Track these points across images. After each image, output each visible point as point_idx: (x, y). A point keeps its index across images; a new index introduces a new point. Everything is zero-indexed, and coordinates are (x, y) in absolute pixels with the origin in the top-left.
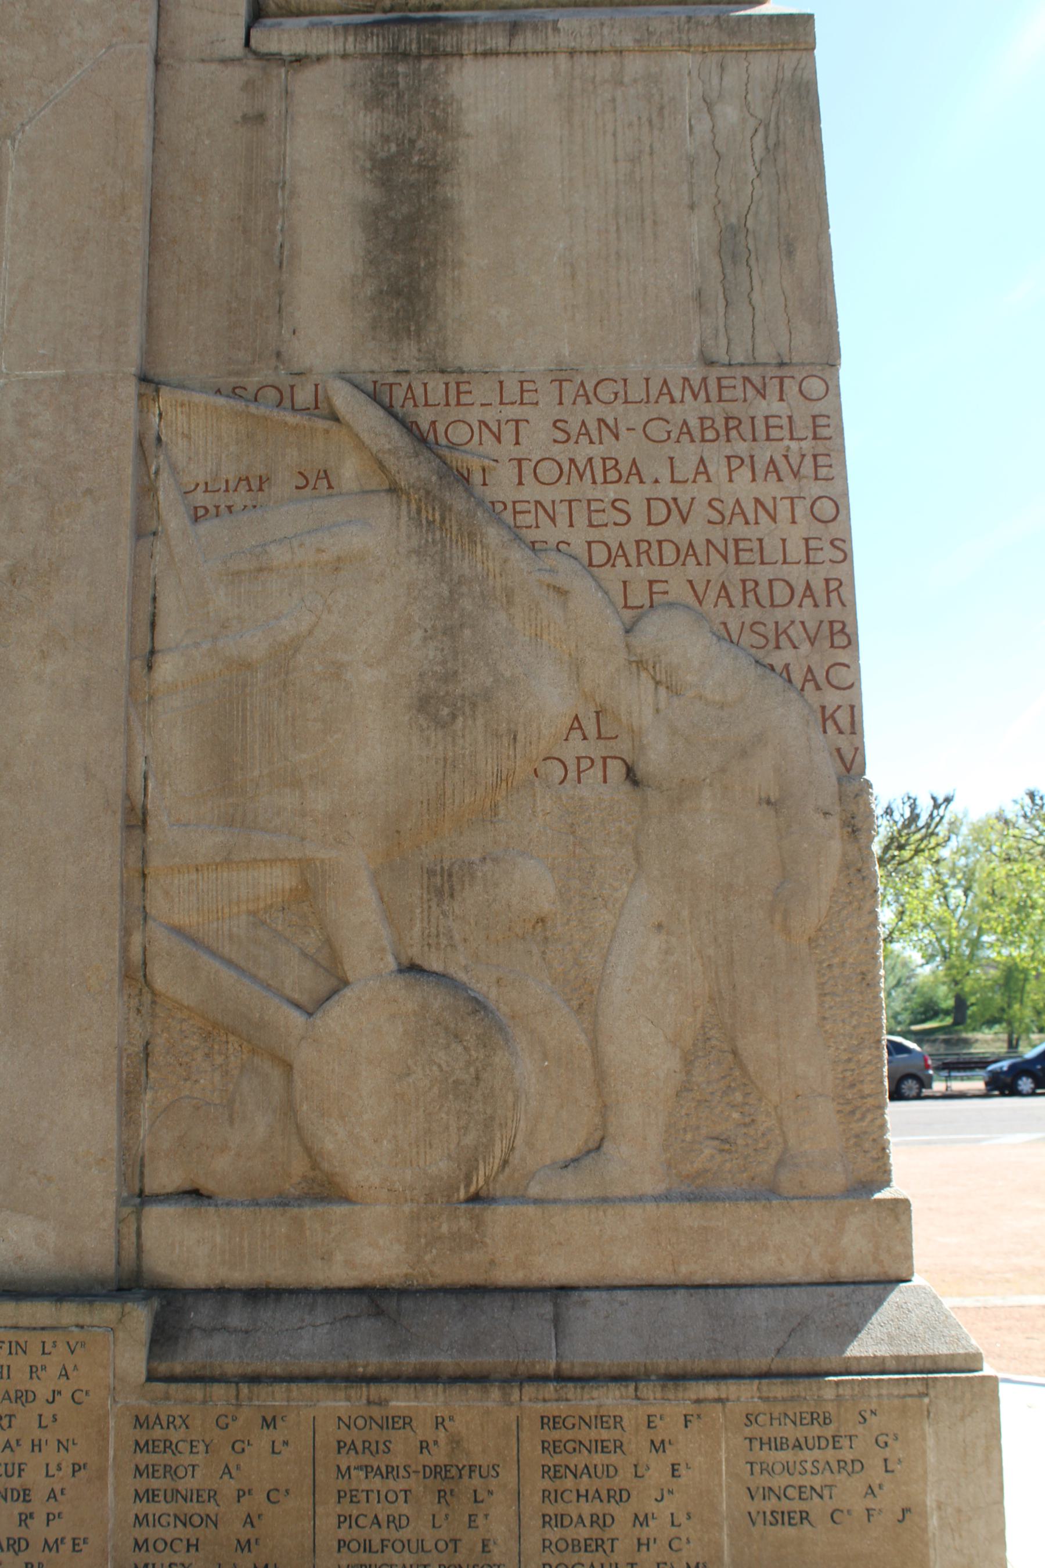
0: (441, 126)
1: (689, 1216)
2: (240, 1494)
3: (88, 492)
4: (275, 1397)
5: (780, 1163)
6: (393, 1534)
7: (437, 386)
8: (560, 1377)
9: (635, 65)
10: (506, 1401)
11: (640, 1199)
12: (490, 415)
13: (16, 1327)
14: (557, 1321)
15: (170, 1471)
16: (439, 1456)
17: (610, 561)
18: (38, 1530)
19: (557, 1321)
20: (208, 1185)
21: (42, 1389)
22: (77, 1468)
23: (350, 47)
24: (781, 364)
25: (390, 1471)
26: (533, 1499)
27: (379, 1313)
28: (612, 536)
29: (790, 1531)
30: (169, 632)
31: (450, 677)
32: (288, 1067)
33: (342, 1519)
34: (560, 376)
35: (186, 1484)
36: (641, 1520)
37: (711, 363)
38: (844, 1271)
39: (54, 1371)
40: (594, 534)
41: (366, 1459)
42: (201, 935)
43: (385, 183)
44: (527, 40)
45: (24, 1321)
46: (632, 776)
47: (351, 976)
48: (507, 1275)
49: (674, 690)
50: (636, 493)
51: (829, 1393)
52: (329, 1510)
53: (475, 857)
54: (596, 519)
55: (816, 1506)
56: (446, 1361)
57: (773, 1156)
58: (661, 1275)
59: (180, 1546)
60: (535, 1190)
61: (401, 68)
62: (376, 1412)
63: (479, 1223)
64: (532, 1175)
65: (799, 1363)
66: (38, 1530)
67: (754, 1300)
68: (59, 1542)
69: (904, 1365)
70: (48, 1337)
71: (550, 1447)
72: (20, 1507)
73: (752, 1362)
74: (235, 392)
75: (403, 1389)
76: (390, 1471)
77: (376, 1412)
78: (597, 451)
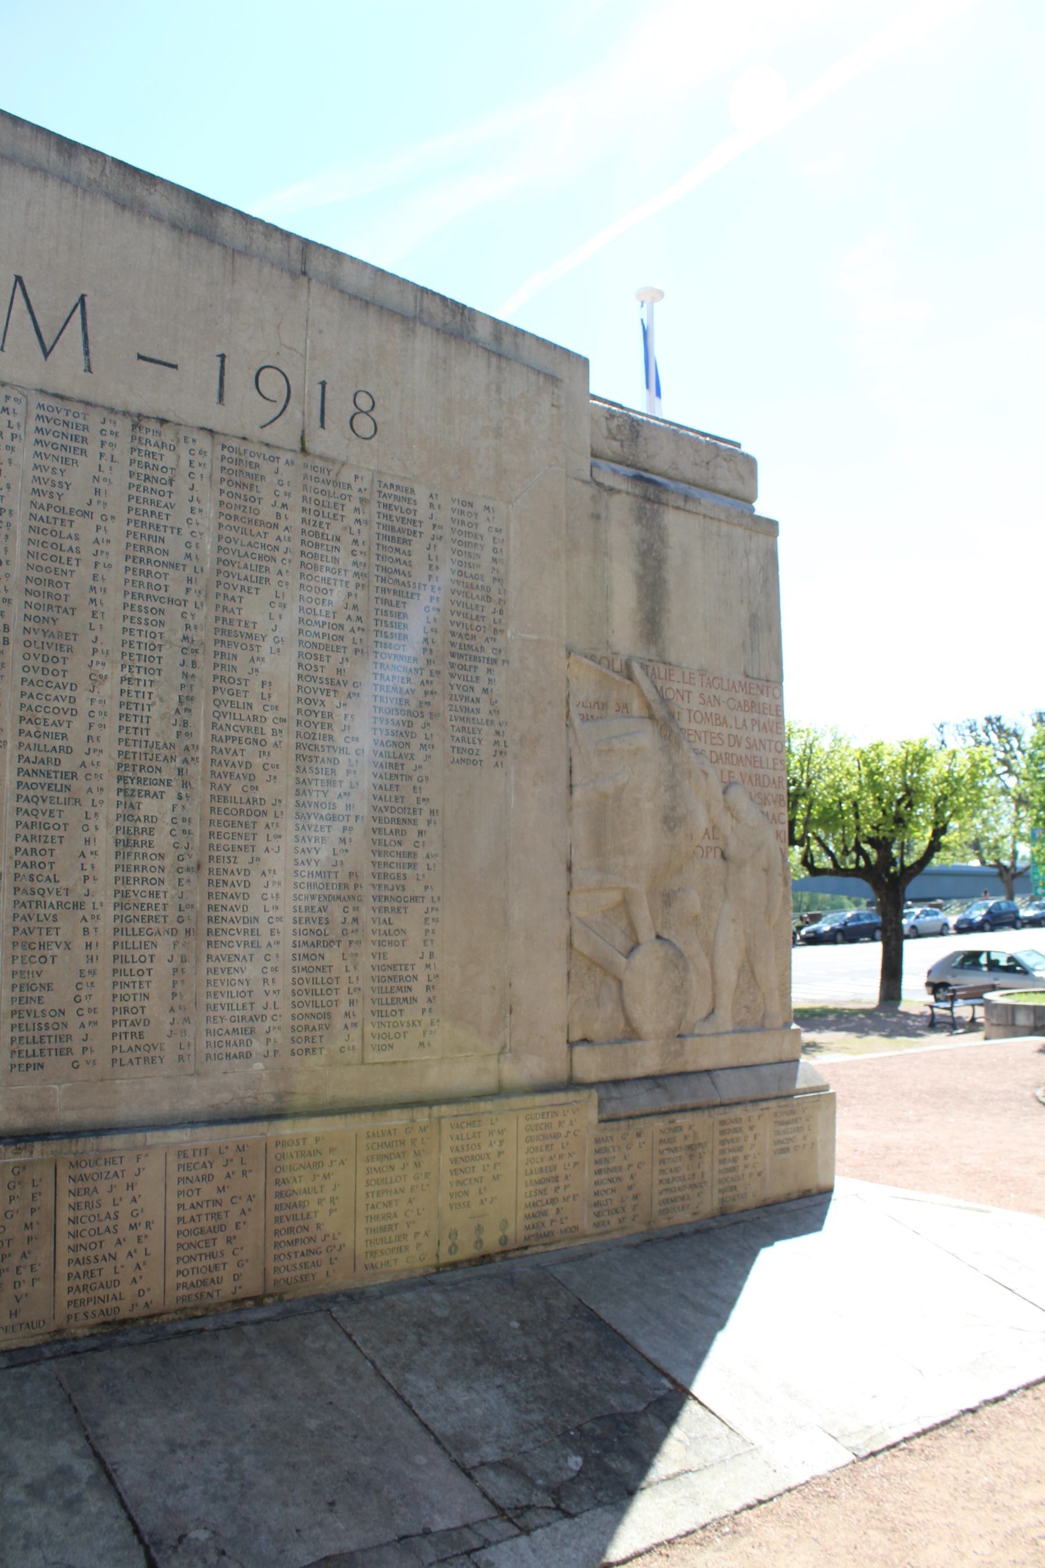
0: (662, 540)
1: (742, 1038)
2: (630, 1166)
3: (549, 703)
4: (640, 1124)
5: (764, 1016)
6: (675, 1175)
7: (662, 668)
8: (722, 1105)
9: (725, 528)
10: (710, 1116)
11: (727, 1033)
12: (680, 686)
13: (552, 1105)
14: (713, 1083)
15: (607, 1160)
16: (689, 1142)
17: (717, 761)
18: (562, 1193)
19: (713, 1083)
20: (591, 1036)
21: (563, 1132)
22: (575, 1164)
23: (630, 490)
24: (768, 681)
25: (675, 1150)
26: (716, 1153)
27: (659, 1086)
28: (718, 749)
29: (783, 1156)
30: (577, 778)
31: (673, 809)
32: (620, 983)
33: (662, 1171)
34: (703, 672)
35: (612, 1165)
36: (746, 1158)
37: (747, 676)
38: (784, 1058)
39: (567, 1122)
40: (713, 748)
41: (668, 1146)
42: (905, 911)
43: (643, 563)
44: (690, 506)
45: (555, 1102)
46: (724, 856)
47: (641, 940)
48: (690, 1067)
49: (738, 820)
50: (725, 731)
51: (795, 1102)
52: (657, 1167)
53: (676, 888)
54: (714, 741)
55: (791, 1145)
56: (689, 1102)
57: (761, 1014)
58: (735, 1063)
59: (609, 1192)
60: (696, 1031)
61: (648, 506)
62: (672, 1126)
63: (682, 1045)
64: (695, 1025)
65: (785, 1093)
66: (562, 1193)
67: (764, 1070)
68: (569, 1197)
69: (812, 1090)
70: (565, 1108)
71: (722, 1132)
72: (555, 1184)
73: (774, 1094)
74: (592, 658)
75: (680, 1115)
76: (675, 1150)
77: (672, 1126)
78: (713, 710)
